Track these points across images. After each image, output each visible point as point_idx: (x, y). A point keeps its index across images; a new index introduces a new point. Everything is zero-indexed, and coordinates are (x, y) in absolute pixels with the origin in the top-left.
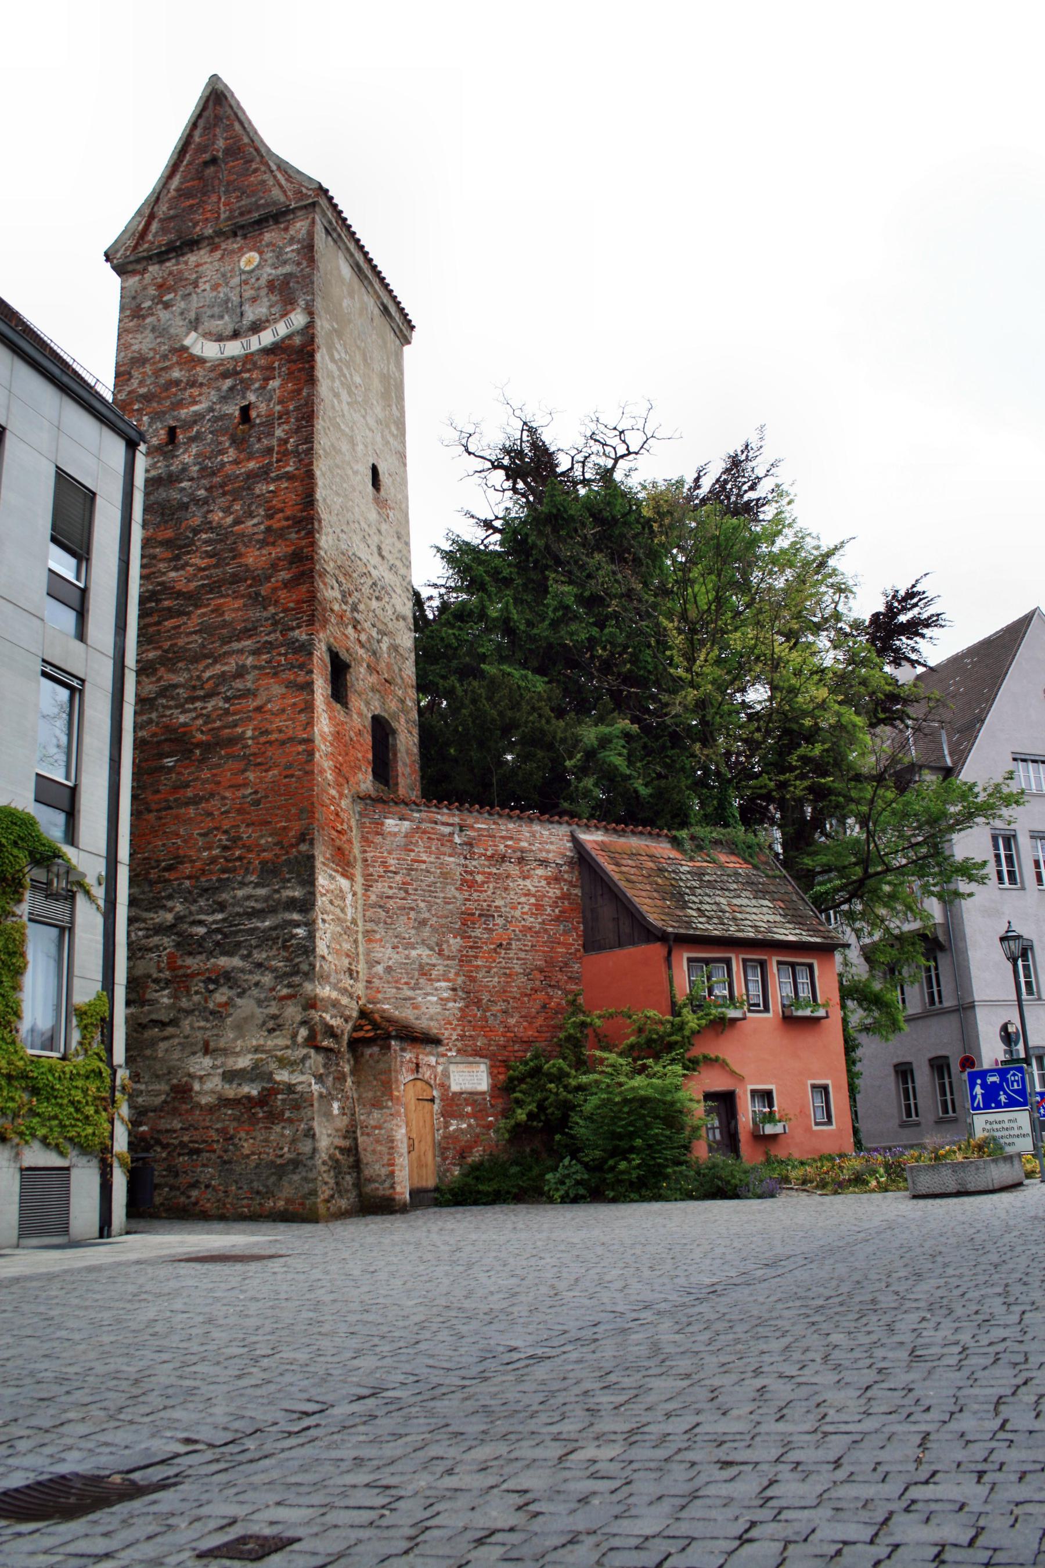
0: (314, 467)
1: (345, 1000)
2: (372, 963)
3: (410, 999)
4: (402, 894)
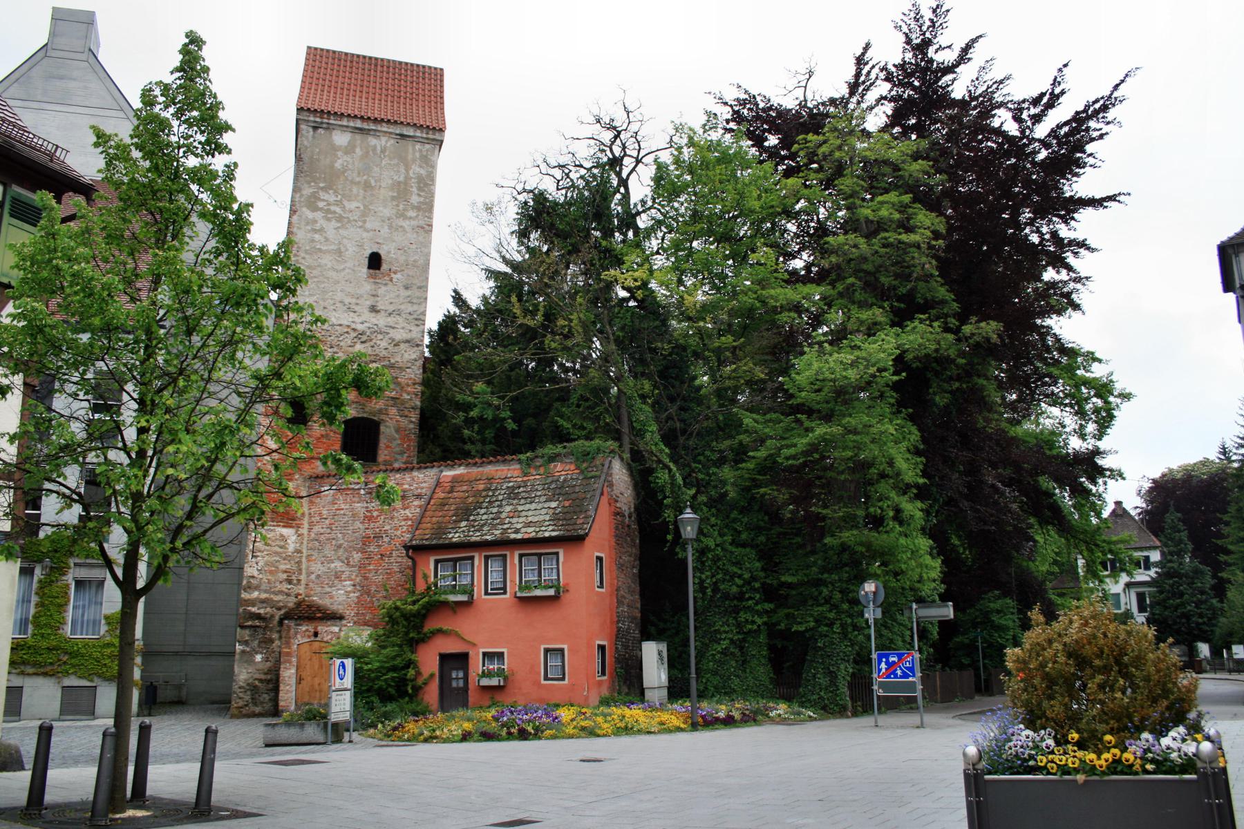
2: (309, 574)
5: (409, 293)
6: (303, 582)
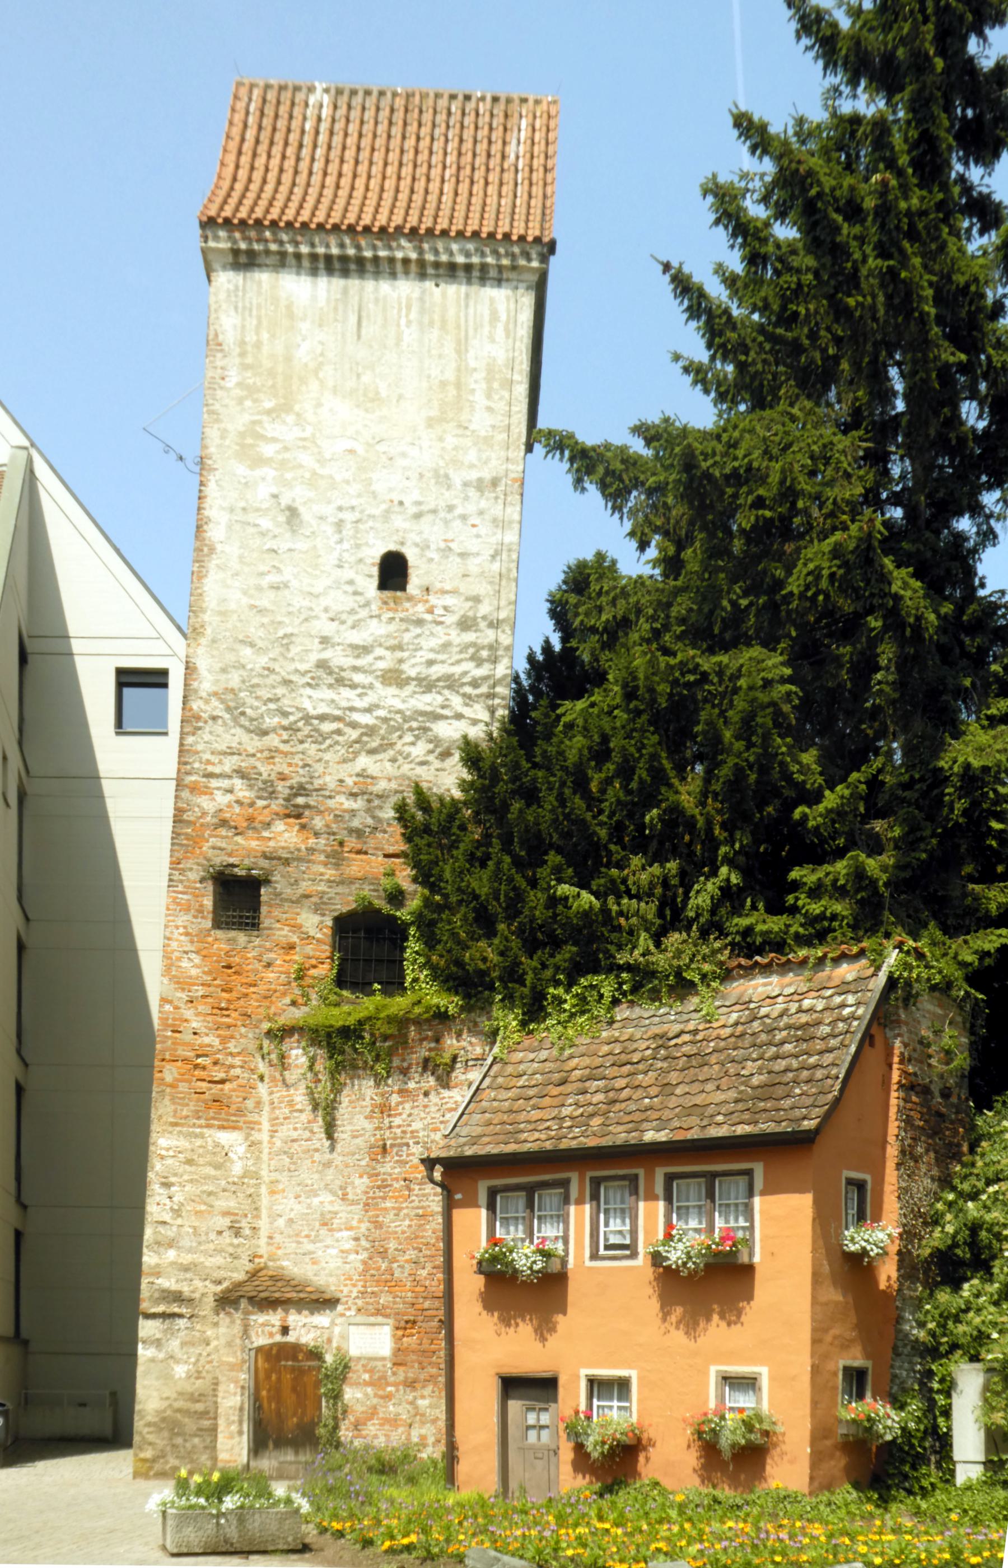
3: (311, 1253)
5: (470, 637)
6: (263, 1233)
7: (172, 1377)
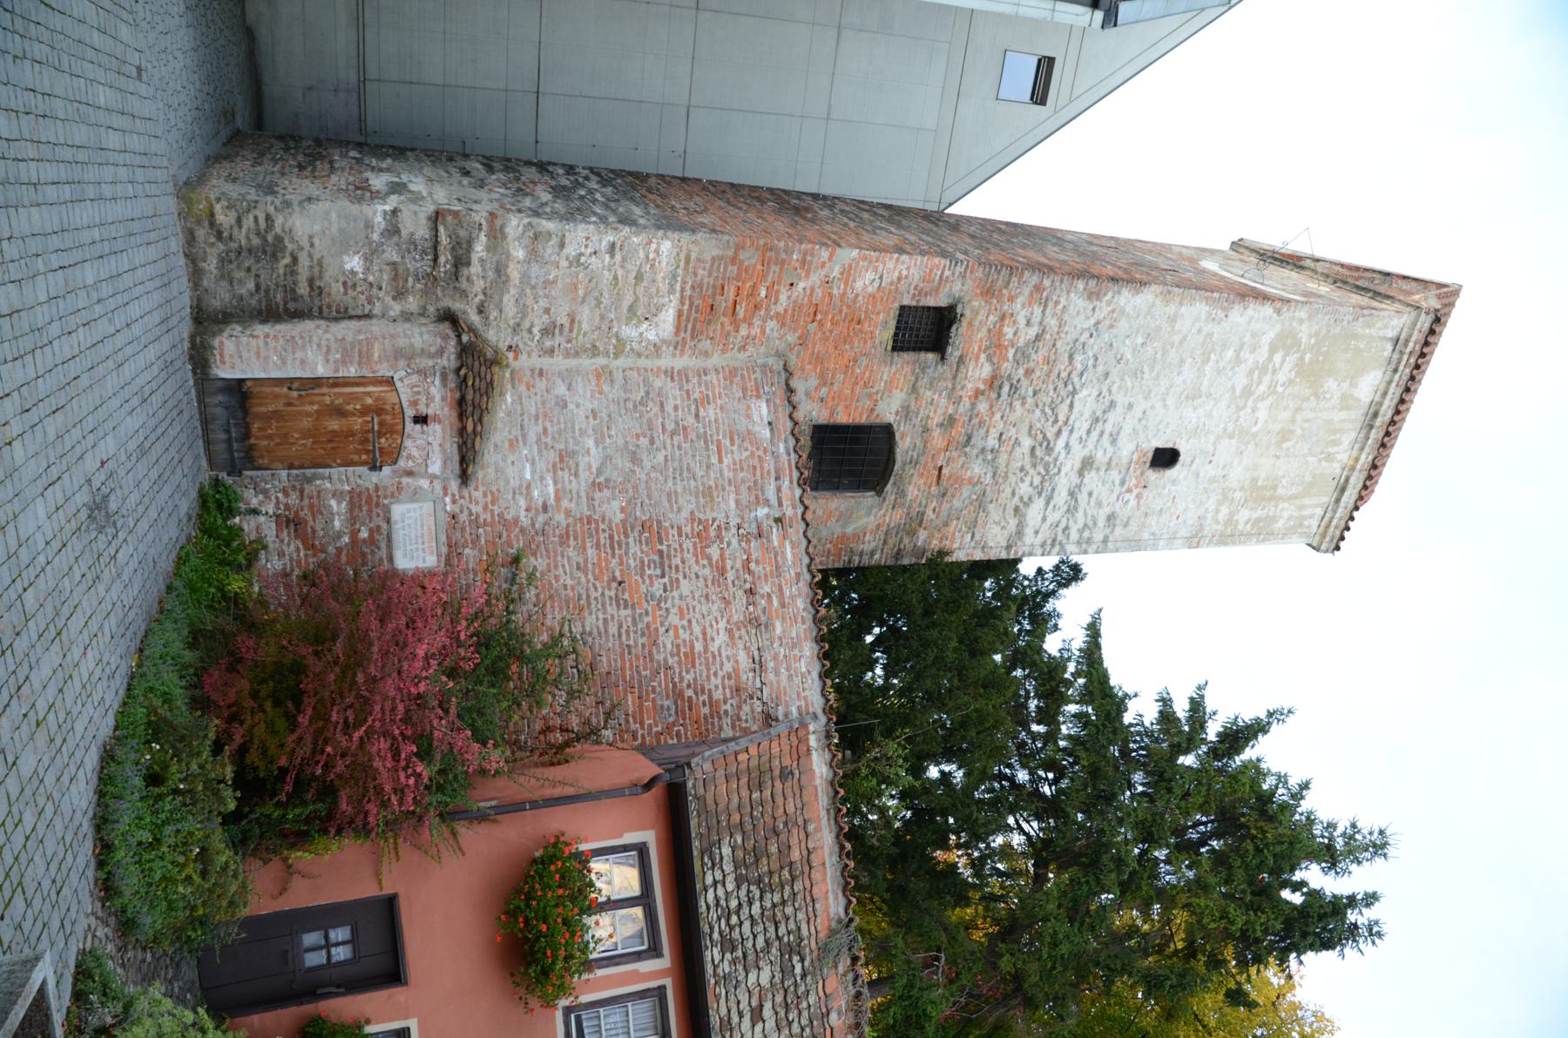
0: (1154, 287)
1: (508, 301)
3: (524, 436)
4: (670, 426)
5: (1101, 522)
6: (546, 362)
7: (345, 252)
